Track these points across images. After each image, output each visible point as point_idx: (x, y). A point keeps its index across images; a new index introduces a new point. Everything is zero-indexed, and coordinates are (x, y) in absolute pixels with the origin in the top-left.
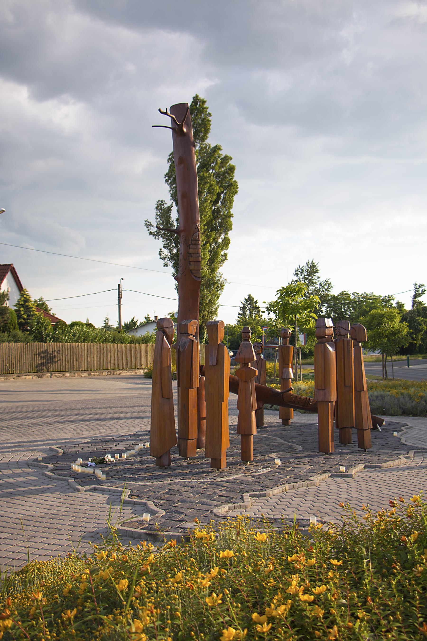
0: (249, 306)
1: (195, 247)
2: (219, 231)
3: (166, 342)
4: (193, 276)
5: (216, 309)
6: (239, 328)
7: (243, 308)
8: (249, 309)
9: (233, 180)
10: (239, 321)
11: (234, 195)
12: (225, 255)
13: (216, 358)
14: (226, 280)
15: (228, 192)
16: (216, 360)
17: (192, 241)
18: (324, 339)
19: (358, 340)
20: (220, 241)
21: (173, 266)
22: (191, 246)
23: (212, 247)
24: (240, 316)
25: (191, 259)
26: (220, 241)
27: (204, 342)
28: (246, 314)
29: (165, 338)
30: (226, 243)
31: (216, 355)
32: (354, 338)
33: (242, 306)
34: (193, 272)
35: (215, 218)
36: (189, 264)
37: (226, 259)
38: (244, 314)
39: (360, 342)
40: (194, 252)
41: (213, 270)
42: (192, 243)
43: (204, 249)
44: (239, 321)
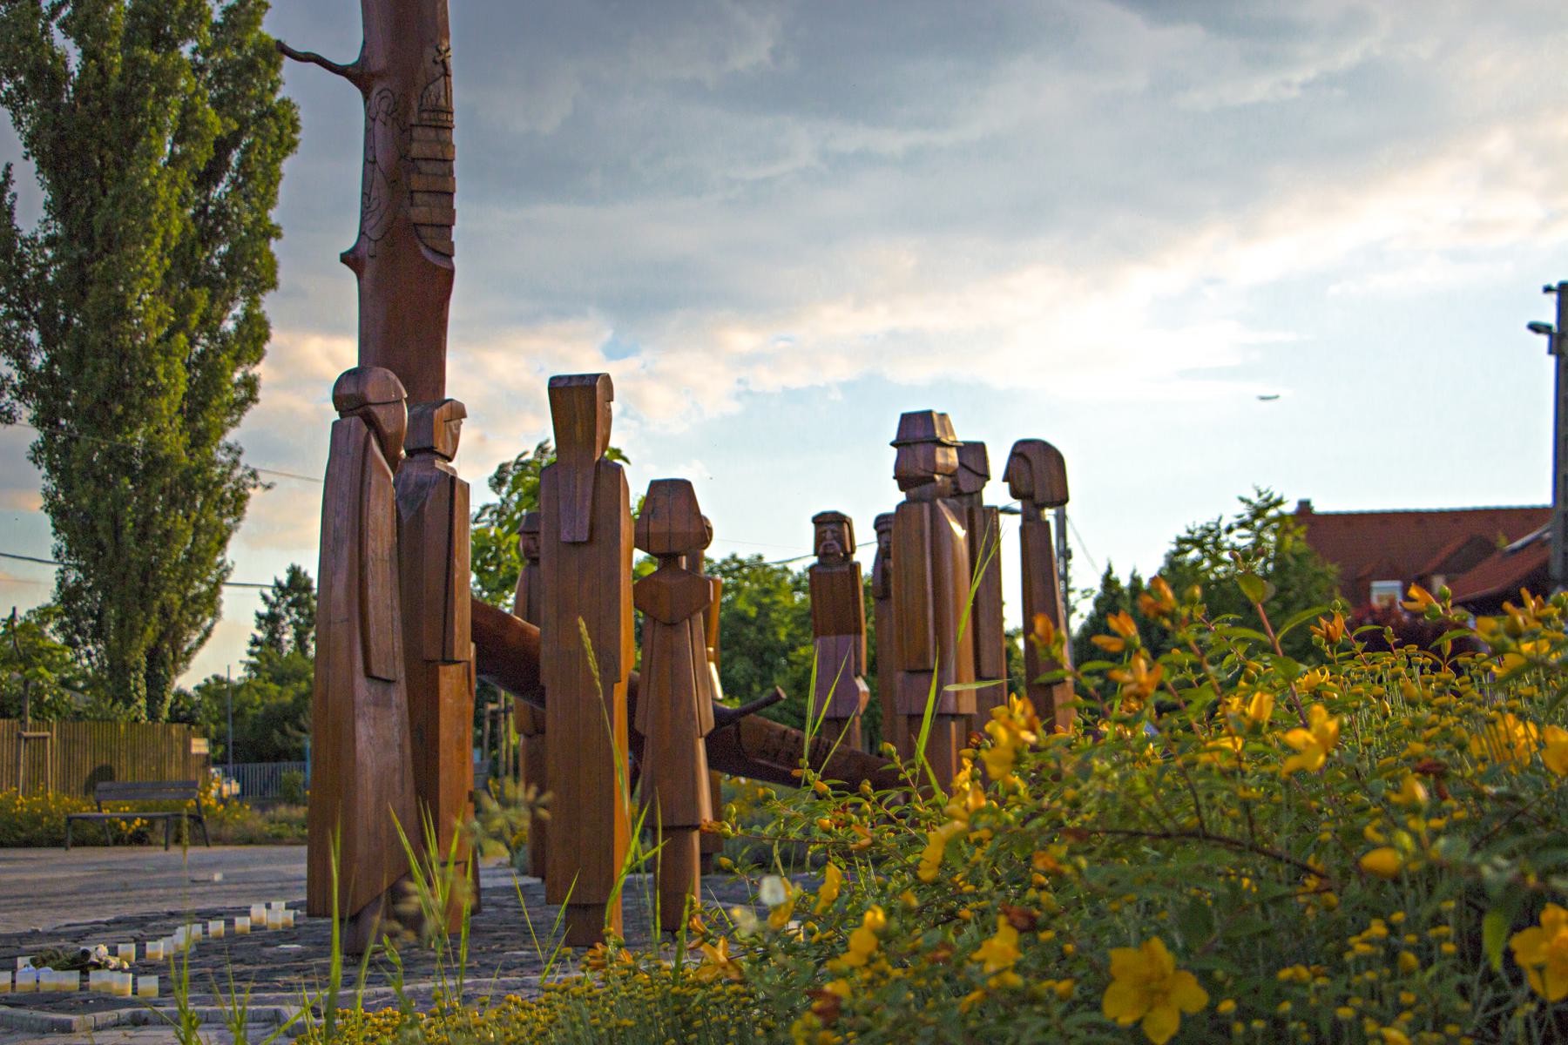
0: (293, 611)
1: (432, 134)
2: (224, 286)
3: (379, 461)
4: (424, 251)
5: (215, 589)
6: (258, 690)
7: (270, 621)
8: (296, 624)
9: (279, 96)
10: (252, 666)
11: (285, 155)
12: (251, 384)
13: (587, 513)
14: (254, 475)
15: (259, 140)
16: (587, 522)
17: (421, 111)
18: (928, 488)
19: (1038, 499)
20: (229, 325)
21: (37, 422)
22: (417, 132)
23: (199, 348)
24: (257, 649)
25: (417, 182)
26: (229, 325)
27: (166, 715)
28: (279, 641)
29: (374, 442)
30: (254, 336)
31: (588, 503)
32: (1023, 490)
33: (265, 610)
34: (424, 231)
35: (207, 238)
36: (407, 202)
37: (252, 398)
38: (274, 641)
39: (1043, 506)
40: (429, 154)
41: (200, 440)
42: (421, 119)
43: (167, 353)
44: (252, 666)
